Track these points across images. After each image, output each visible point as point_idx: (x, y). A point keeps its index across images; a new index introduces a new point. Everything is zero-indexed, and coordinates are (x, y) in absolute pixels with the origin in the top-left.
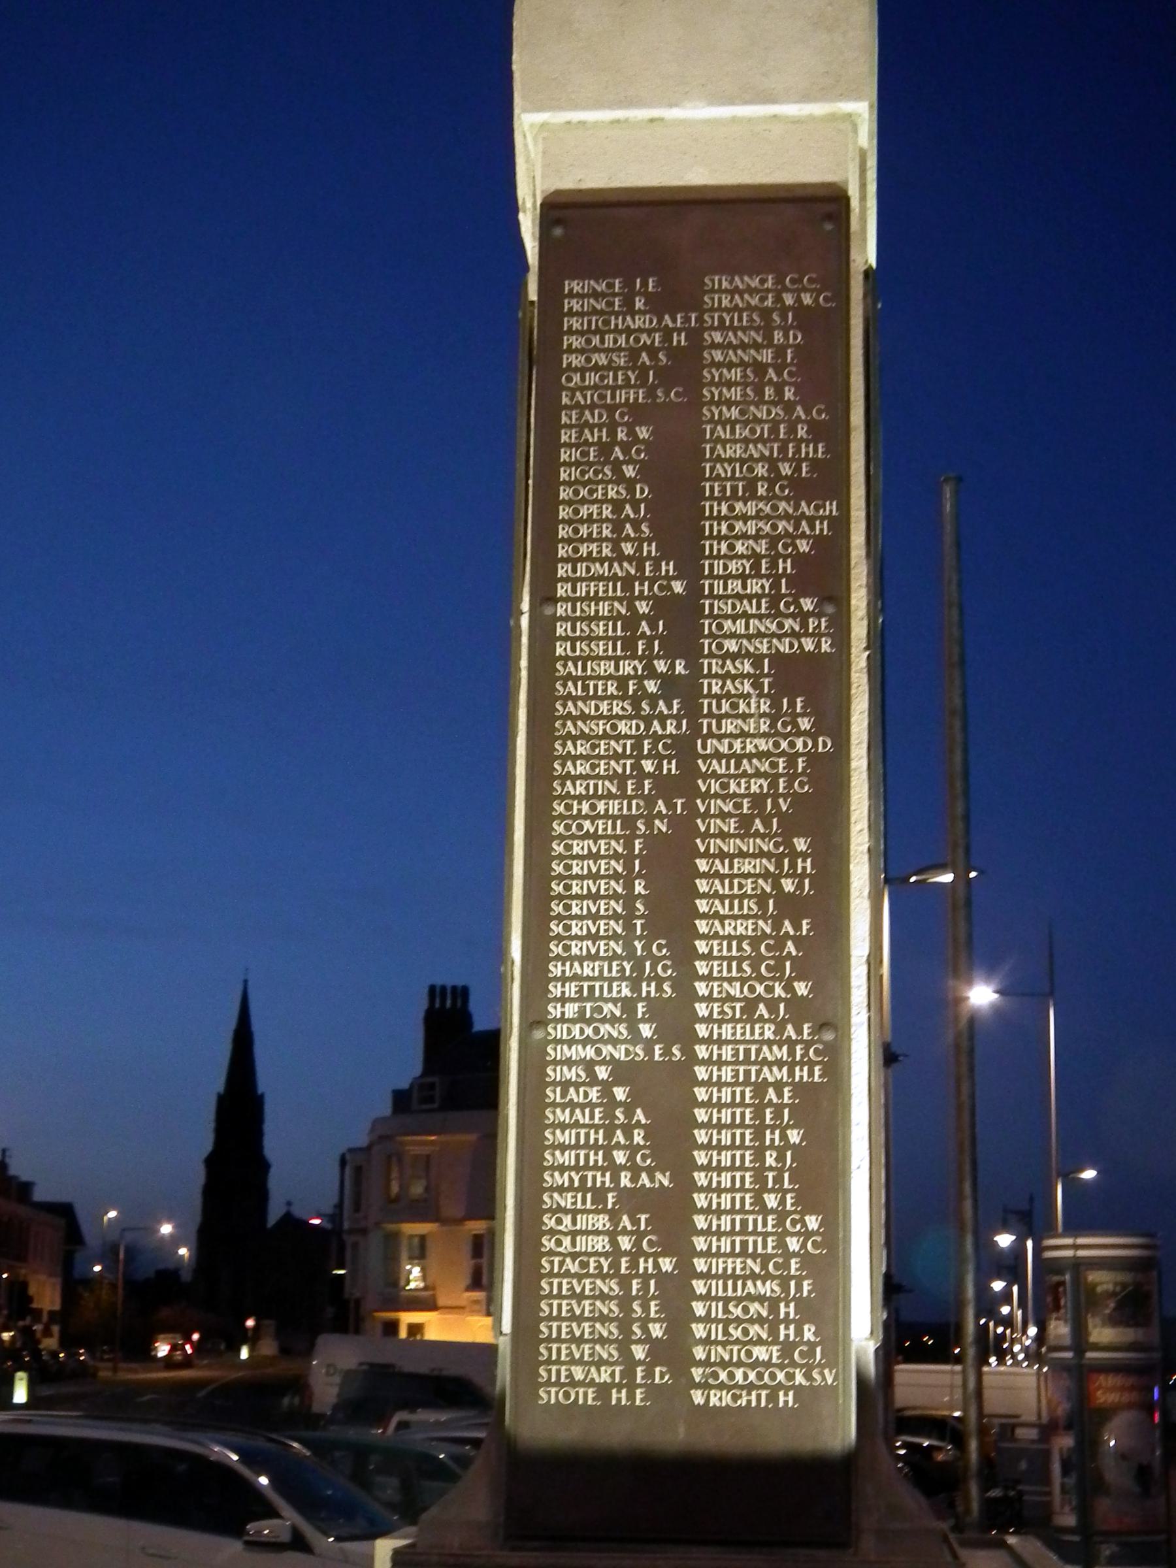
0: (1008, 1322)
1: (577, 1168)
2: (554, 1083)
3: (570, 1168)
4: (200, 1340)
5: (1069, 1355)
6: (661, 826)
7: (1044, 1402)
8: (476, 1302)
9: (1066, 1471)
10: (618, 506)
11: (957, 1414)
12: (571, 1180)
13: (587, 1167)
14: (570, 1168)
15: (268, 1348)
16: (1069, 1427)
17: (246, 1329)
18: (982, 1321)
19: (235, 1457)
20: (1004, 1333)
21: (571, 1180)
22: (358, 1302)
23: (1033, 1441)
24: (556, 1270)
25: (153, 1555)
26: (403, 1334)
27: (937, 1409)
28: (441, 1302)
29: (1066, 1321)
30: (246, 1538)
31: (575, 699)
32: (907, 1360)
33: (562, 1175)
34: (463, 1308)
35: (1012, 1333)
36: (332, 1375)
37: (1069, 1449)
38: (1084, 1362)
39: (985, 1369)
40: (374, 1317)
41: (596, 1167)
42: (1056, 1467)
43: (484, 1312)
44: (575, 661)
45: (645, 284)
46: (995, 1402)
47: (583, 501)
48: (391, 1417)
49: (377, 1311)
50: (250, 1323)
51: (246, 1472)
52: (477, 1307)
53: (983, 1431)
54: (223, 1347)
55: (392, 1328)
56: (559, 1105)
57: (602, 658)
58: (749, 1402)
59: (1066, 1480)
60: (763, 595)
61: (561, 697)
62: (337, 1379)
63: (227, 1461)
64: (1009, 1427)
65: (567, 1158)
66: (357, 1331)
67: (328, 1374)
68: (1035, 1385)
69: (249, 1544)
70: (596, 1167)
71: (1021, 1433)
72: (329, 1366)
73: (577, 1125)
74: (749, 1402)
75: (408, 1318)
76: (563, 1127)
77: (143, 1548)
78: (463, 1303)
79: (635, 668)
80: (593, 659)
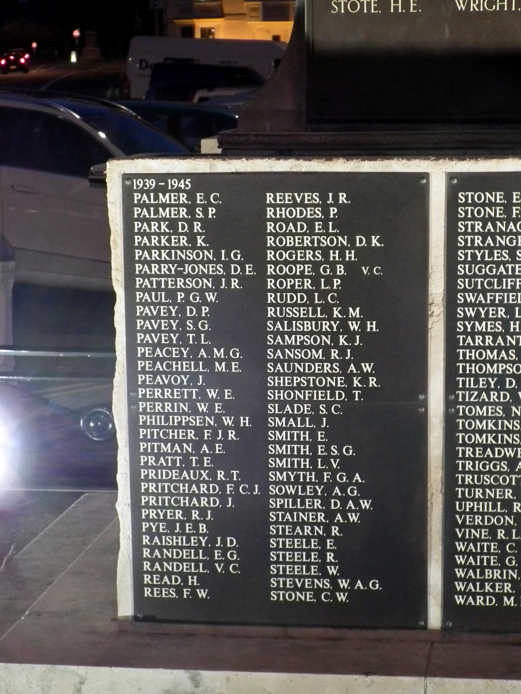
1: (292, 470)
3: (287, 470)
4: (38, 48)
6: (353, 518)
8: (254, 10)
12: (288, 476)
14: (287, 470)
15: (93, 51)
17: (74, 38)
19: (78, 117)
21: (288, 476)
22: (161, 12)
24: (280, 520)
25: (19, 191)
26: (198, 35)
28: (226, 10)
30: (91, 177)
33: (281, 474)
34: (245, 14)
36: (145, 68)
40: (175, 23)
43: (261, 18)
48: (194, 94)
49: (178, 18)
50: (76, 33)
51: (86, 127)
52: (254, 14)
54: (56, 53)
55: (189, 31)
56: (277, 415)
60: (460, 500)
62: (148, 72)
63: (70, 118)
65: (282, 463)
66: (161, 34)
67: (141, 68)
69: (91, 181)
72: (141, 61)
73: (291, 428)
75: (201, 24)
76: (281, 429)
77: (12, 187)
78: (244, 11)
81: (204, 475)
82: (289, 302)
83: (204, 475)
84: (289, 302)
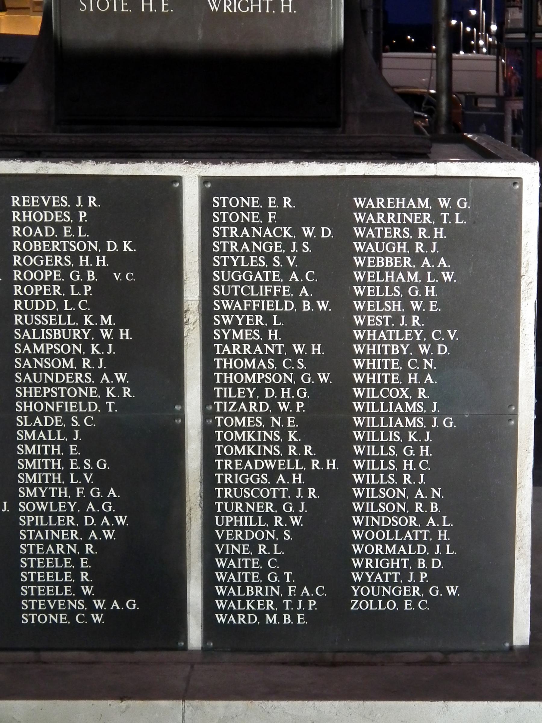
0: (474, 22)
1: (43, 485)
2: (22, 413)
5: (523, 35)
7: (501, 81)
9: (516, 129)
10: (65, 271)
11: (433, 91)
12: (39, 492)
13: (50, 484)
16: (519, 94)
18: (454, 22)
20: (472, 31)
21: (39, 492)
23: (491, 109)
27: (417, 88)
29: (520, 8)
31: (31, 343)
32: (394, 49)
35: (478, 31)
37: (519, 111)
38: (534, 41)
39: (455, 55)
41: (57, 485)
42: (509, 127)
44: (30, 329)
45: (85, 201)
46: (462, 82)
47: (33, 283)
53: (451, 103)
56: (26, 428)
57: (53, 327)
58: (256, 9)
59: (516, 135)
61: (19, 341)
64: (472, 99)
68: (494, 69)
70: (57, 485)
71: (483, 104)
74: (256, 9)
76: (30, 443)
79: (82, 335)
80: (46, 327)
81: (404, 393)
82: (37, 309)
83: (404, 393)
84: (37, 309)
